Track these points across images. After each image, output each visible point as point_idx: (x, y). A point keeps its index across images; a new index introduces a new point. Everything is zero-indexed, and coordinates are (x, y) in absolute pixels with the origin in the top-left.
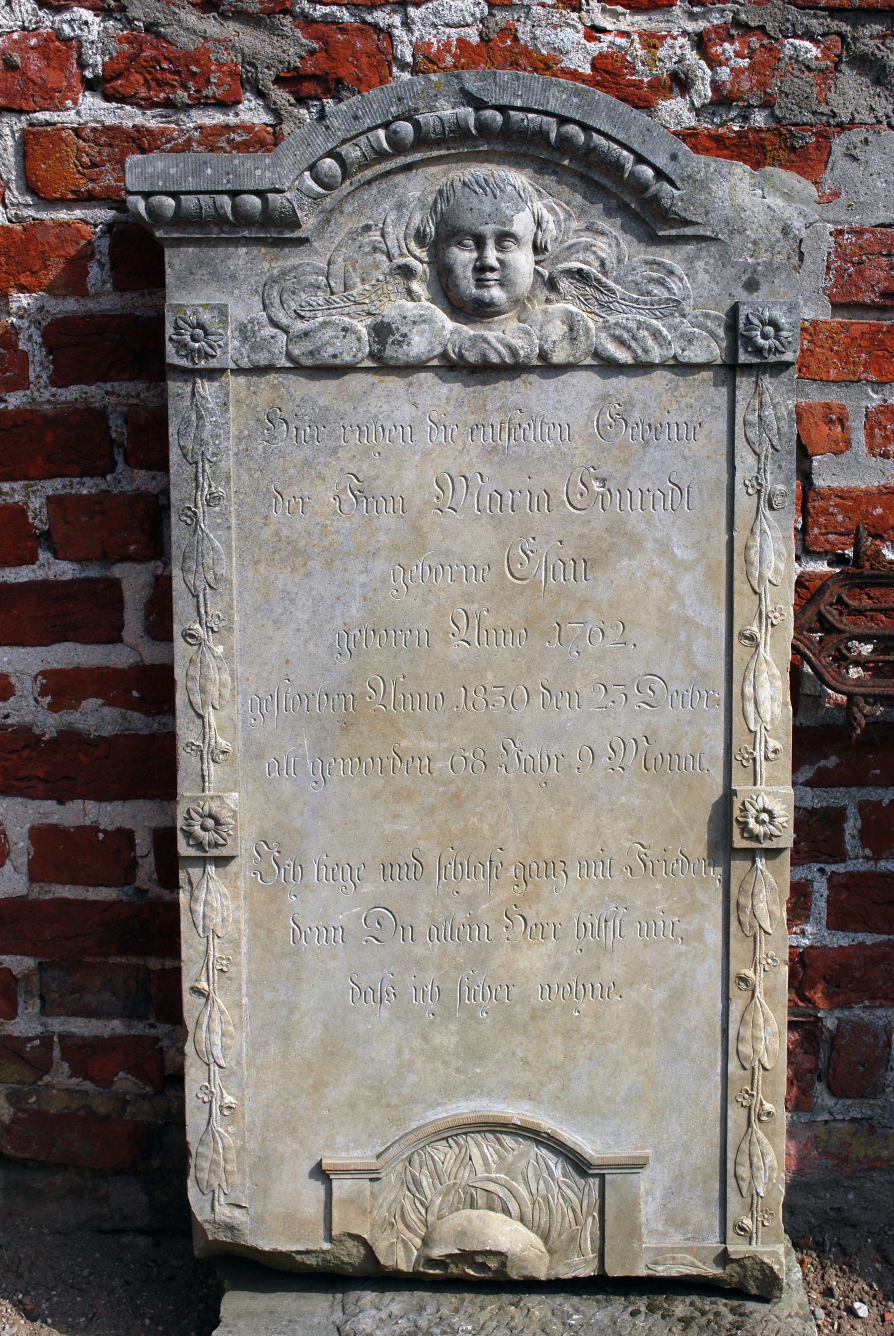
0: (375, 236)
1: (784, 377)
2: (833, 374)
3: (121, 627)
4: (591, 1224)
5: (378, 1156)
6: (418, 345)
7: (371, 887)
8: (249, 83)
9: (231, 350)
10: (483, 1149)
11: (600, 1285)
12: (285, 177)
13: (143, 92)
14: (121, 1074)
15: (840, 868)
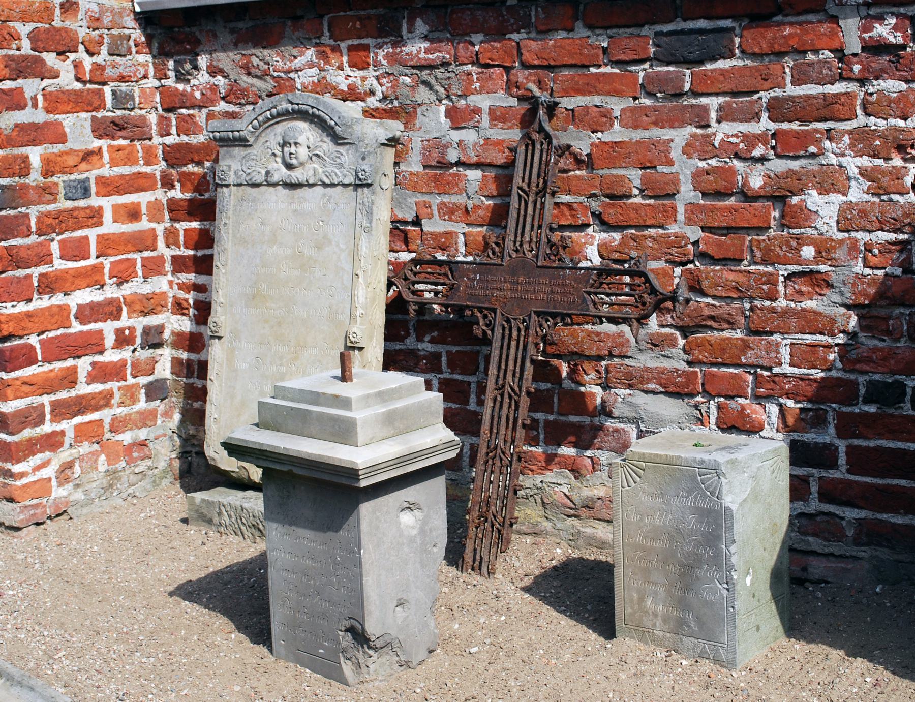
0: (268, 144)
2: (424, 190)
6: (276, 178)
12: (243, 127)
15: (441, 376)
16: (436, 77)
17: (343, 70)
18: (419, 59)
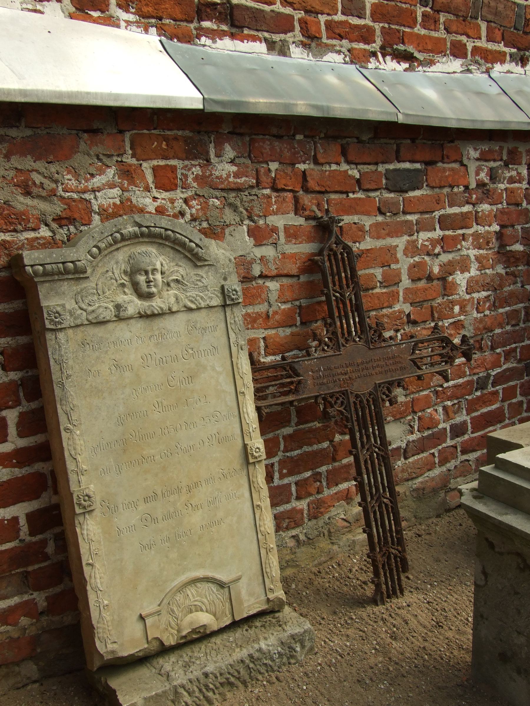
0: (110, 274)
1: (239, 307)
3: (7, 435)
4: (228, 605)
5: (159, 605)
6: (131, 310)
7: (142, 507)
8: (43, 221)
9: (69, 321)
10: (191, 591)
11: (235, 625)
13: (4, 227)
14: (22, 618)
16: (242, 201)
17: (149, 191)
18: (229, 182)
